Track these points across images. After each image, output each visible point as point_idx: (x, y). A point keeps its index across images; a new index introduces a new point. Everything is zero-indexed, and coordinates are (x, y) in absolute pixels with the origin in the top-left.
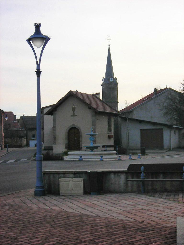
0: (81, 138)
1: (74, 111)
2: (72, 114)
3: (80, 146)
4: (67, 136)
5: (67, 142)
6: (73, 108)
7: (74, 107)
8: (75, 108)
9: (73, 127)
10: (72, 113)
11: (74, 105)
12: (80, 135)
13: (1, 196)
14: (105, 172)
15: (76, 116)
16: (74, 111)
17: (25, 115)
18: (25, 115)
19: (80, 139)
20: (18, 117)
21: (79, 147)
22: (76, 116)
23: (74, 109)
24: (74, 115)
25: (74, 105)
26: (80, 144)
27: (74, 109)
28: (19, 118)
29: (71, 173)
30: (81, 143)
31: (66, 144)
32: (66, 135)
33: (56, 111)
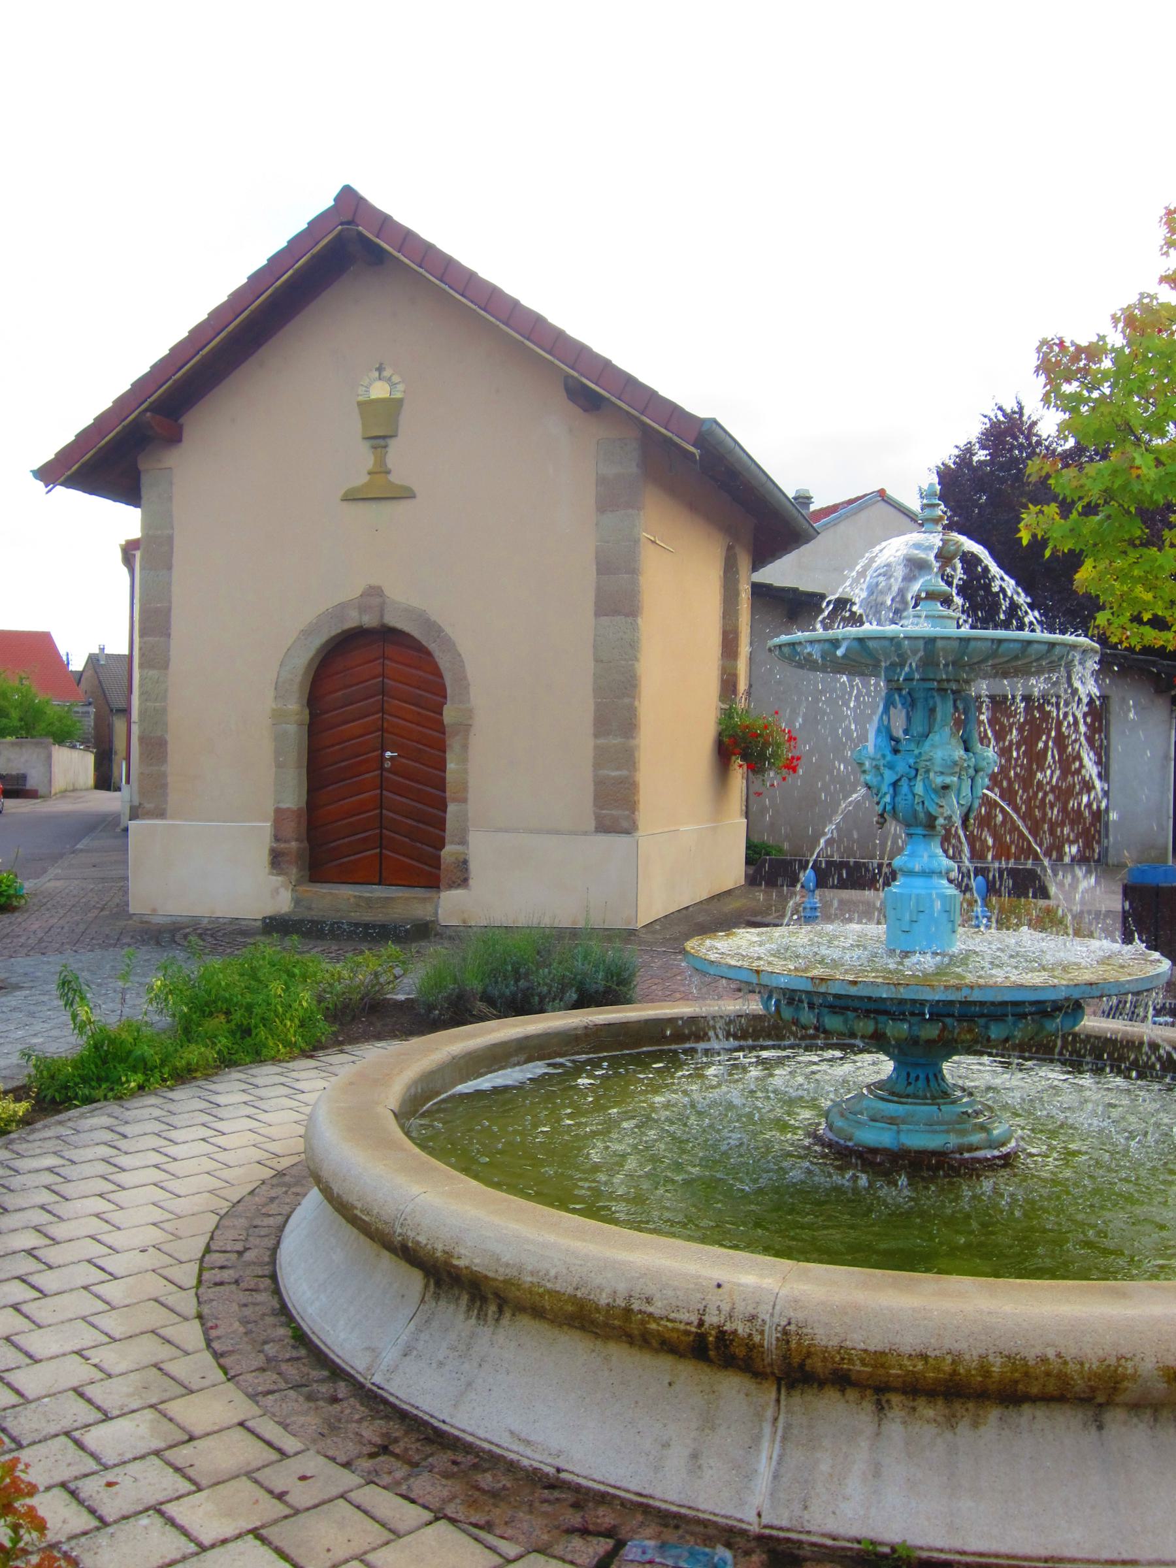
0: (464, 760)
1: (379, 441)
2: (361, 479)
3: (440, 844)
4: (292, 728)
5: (293, 798)
6: (367, 408)
7: (379, 391)
8: (400, 402)
9: (369, 620)
10: (366, 458)
11: (380, 369)
12: (449, 714)
13: (54, 1094)
14: (815, 1256)
15: (406, 494)
16: (379, 441)
17: (106, 652)
18: (106, 652)
19: (451, 766)
20: (77, 664)
21: (436, 862)
22: (406, 494)
23: (381, 426)
24: (380, 491)
25: (380, 369)
26: (450, 824)
27: (381, 426)
28: (80, 669)
29: (142, 1333)
30: (451, 808)
31: (280, 816)
32: (278, 716)
33: (174, 438)
